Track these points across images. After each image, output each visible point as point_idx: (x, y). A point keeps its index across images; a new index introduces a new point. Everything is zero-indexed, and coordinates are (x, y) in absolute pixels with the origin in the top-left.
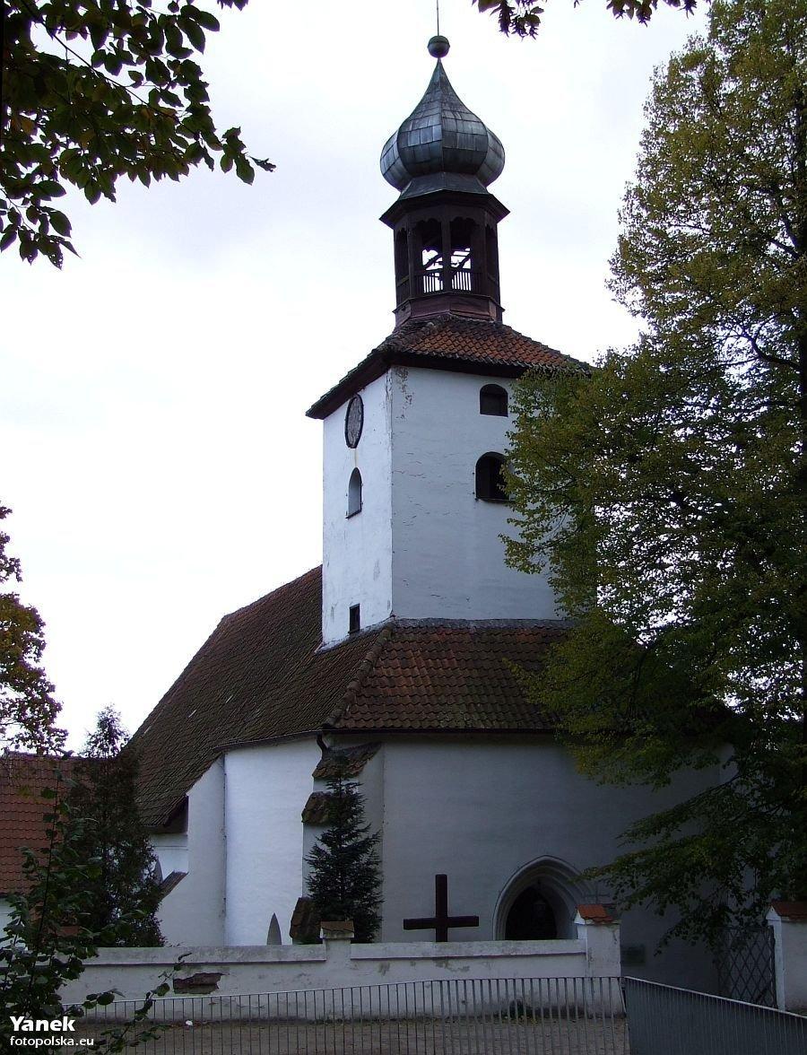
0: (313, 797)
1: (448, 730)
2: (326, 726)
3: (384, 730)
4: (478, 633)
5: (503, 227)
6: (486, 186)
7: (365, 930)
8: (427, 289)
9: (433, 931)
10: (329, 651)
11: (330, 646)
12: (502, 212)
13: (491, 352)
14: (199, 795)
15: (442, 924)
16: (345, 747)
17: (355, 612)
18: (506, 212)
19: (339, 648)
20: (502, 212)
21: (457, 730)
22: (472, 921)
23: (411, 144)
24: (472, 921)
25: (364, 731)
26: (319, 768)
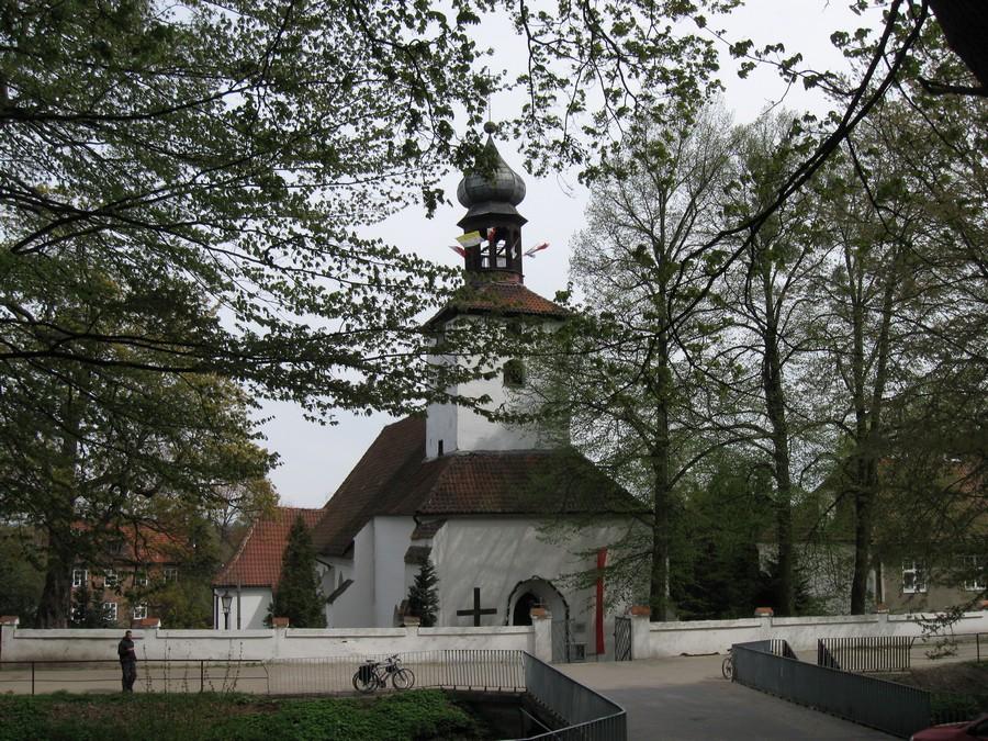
0: (411, 548)
1: (481, 513)
2: (417, 512)
3: (447, 513)
4: (503, 458)
5: (524, 229)
6: (515, 206)
7: (428, 621)
8: (505, 265)
9: (472, 617)
10: (431, 462)
11: (430, 460)
12: (524, 221)
13: (513, 304)
14: (360, 539)
15: (477, 613)
16: (428, 522)
17: (441, 443)
18: (525, 221)
19: (433, 462)
20: (524, 221)
21: (486, 513)
22: (493, 611)
23: (473, 185)
24: (493, 611)
25: (438, 514)
26: (414, 533)
